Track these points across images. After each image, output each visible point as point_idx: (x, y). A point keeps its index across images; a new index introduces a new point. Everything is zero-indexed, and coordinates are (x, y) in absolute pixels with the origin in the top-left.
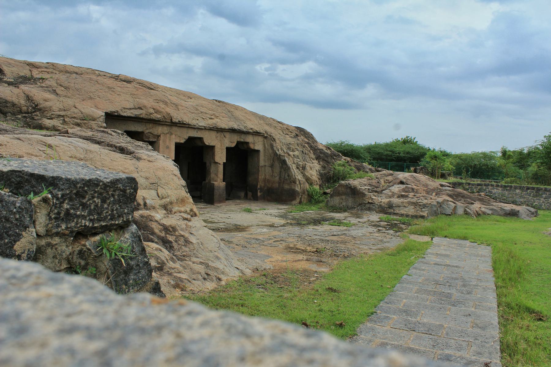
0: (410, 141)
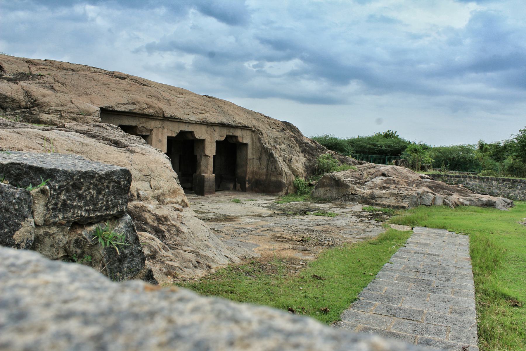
0: (392, 135)
